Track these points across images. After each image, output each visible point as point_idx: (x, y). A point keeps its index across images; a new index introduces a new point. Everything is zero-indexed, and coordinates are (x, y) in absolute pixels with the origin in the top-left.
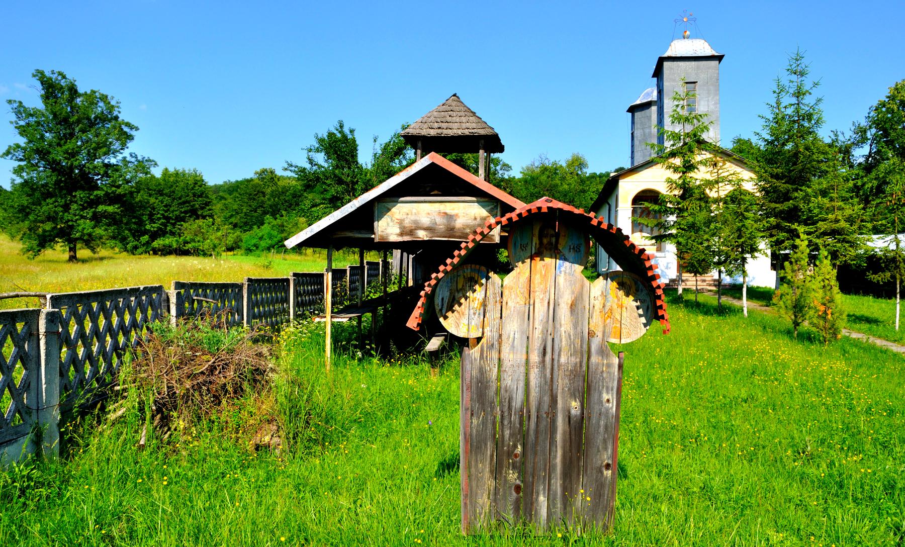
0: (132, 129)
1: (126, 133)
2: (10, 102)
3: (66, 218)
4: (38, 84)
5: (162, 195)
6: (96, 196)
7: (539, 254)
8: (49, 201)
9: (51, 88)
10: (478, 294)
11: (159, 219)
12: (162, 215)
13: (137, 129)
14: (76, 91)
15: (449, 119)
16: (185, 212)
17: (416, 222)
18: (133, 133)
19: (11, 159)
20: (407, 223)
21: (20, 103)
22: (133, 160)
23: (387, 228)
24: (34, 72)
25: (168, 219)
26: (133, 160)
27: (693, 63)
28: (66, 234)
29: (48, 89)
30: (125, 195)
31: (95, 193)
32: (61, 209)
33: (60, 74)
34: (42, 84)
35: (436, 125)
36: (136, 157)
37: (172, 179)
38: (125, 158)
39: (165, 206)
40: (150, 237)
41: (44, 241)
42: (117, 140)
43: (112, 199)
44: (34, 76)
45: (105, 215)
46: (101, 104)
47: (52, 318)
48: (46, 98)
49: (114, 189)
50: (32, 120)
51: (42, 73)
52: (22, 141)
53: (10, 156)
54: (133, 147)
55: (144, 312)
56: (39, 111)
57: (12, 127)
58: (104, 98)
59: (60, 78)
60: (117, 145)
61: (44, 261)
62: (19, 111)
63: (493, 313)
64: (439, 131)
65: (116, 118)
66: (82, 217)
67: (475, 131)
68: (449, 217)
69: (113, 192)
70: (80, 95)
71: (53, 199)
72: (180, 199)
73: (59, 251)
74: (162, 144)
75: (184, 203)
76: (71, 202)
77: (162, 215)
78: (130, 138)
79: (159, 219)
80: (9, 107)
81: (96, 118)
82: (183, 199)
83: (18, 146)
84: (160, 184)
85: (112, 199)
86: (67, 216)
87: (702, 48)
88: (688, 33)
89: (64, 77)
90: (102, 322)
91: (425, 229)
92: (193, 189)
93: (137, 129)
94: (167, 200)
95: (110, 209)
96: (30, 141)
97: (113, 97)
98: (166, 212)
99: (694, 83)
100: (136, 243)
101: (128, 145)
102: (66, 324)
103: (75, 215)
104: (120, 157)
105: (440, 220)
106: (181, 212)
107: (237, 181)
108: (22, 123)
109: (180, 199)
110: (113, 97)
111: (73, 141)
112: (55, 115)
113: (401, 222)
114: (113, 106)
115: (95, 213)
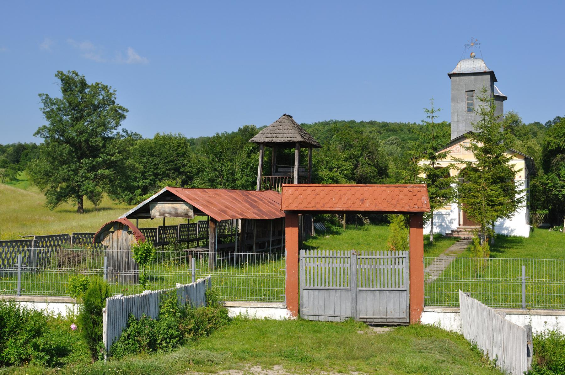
0: (123, 111)
1: (120, 114)
2: (40, 95)
3: (76, 179)
4: (59, 81)
5: (153, 156)
6: (97, 162)
7: (119, 229)
8: (64, 166)
9: (69, 84)
10: (108, 237)
11: (150, 176)
12: (152, 172)
13: (127, 111)
14: (85, 84)
15: (278, 131)
16: (170, 169)
17: (164, 211)
18: (125, 113)
19: (40, 137)
20: (162, 211)
21: (47, 95)
22: (125, 134)
23: (155, 212)
24: (56, 73)
25: (156, 175)
26: (125, 134)
27: (472, 77)
28: (74, 191)
29: (66, 85)
30: (116, 162)
31: (96, 159)
32: (72, 173)
33: (74, 72)
34: (62, 80)
35: (270, 135)
36: (127, 132)
37: (161, 143)
38: (118, 133)
39: (155, 165)
40: (142, 190)
41: (60, 197)
42: (113, 119)
43: (109, 165)
44: (56, 76)
45: (103, 177)
46: (103, 92)
47: (35, 241)
48: (65, 91)
49: (109, 157)
50: (55, 107)
51: (62, 73)
52: (47, 124)
53: (39, 135)
54: (125, 124)
55: (62, 241)
56: (60, 100)
57: (41, 112)
58: (105, 88)
59: (74, 75)
60: (113, 123)
61: (60, 212)
62: (47, 101)
63: (111, 241)
64: (271, 139)
65: (114, 102)
66: (87, 178)
67: (290, 139)
68: (176, 209)
69: (109, 159)
70: (88, 87)
71: (67, 166)
72: (166, 159)
73: (70, 204)
74: (142, 121)
75: (169, 162)
76: (80, 167)
77: (152, 172)
78: (123, 117)
79: (150, 176)
80: (39, 99)
81: (99, 103)
82: (168, 159)
83: (45, 127)
84: (152, 148)
85: (109, 165)
86: (77, 178)
87: (479, 65)
88: (473, 54)
89: (77, 75)
90: (52, 243)
91: (168, 213)
92: (176, 150)
93: (127, 111)
94: (156, 160)
95: (107, 172)
96: (52, 124)
97: (111, 87)
98: (155, 169)
99: (473, 91)
100: (131, 195)
101: (121, 123)
102: (39, 243)
103: (82, 177)
104: (115, 132)
105: (172, 210)
106: (167, 170)
107: (233, 133)
108: (48, 110)
109: (166, 159)
110: (111, 87)
111: (82, 122)
112: (70, 104)
113: (159, 211)
114: (111, 94)
115: (96, 176)
